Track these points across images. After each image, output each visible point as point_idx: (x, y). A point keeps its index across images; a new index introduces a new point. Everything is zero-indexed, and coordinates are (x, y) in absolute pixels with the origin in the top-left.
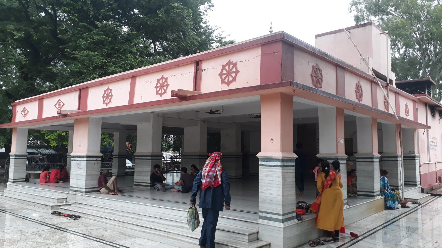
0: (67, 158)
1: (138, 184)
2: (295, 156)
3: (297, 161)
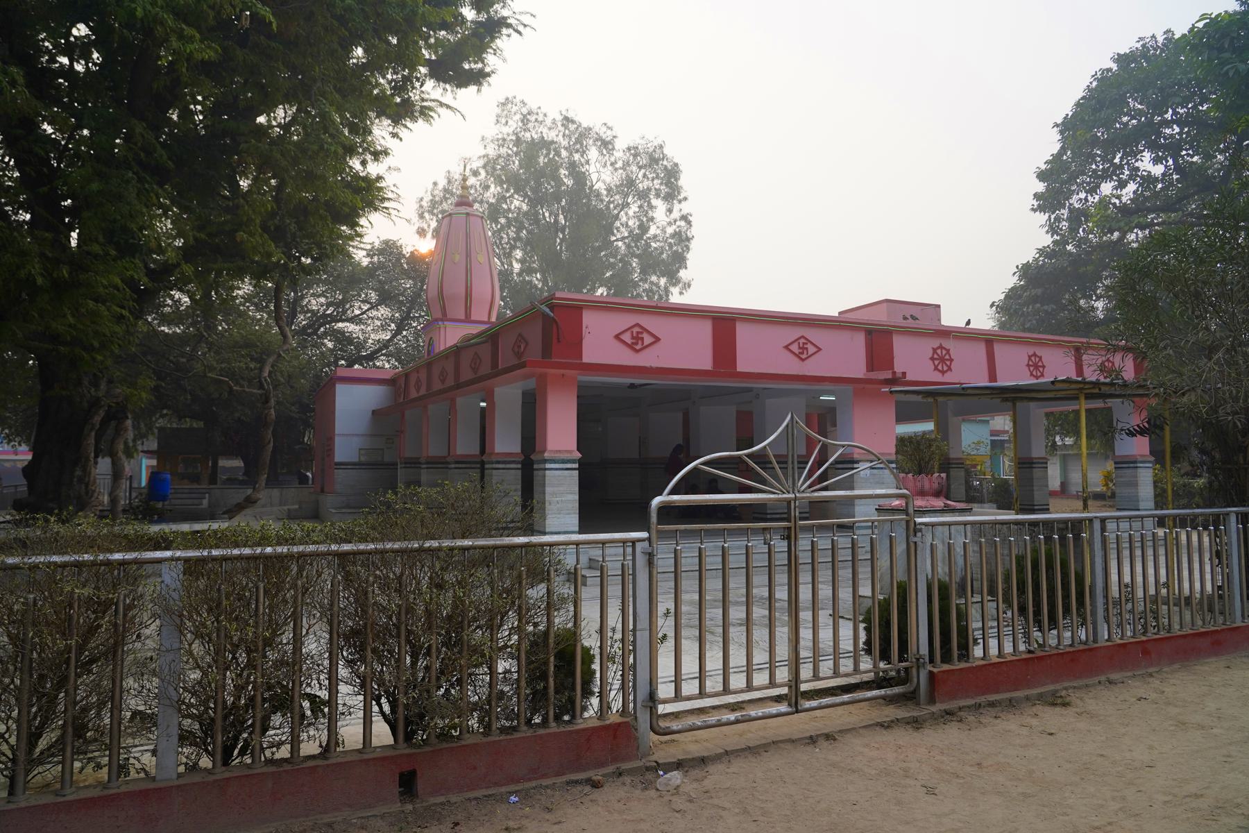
0: (533, 470)
1: (778, 516)
2: (578, 455)
3: (580, 461)
